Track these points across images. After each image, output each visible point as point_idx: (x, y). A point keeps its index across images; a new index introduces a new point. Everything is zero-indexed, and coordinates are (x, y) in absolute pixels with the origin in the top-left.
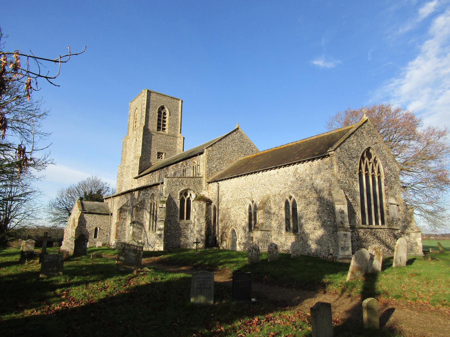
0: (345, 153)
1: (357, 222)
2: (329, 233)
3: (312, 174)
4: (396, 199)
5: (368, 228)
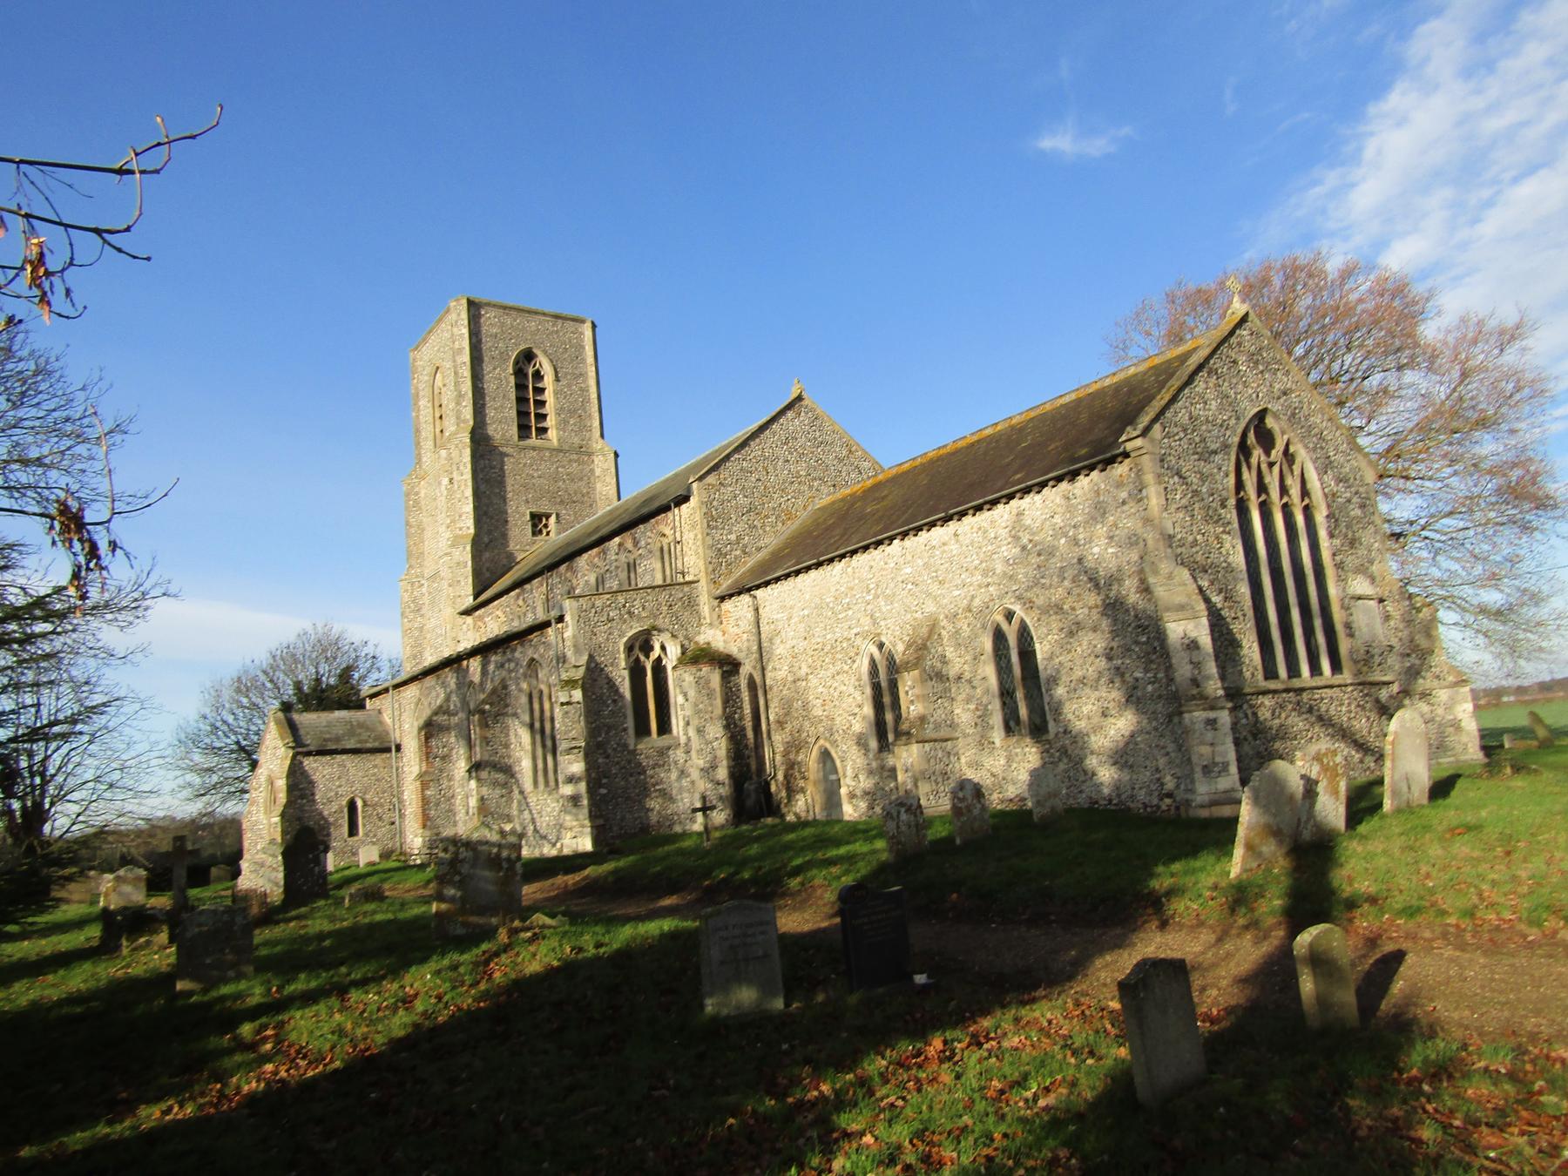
0: (1180, 440)
1: (1247, 675)
2: (1154, 724)
3: (1074, 527)
4: (1373, 579)
5: (1287, 691)
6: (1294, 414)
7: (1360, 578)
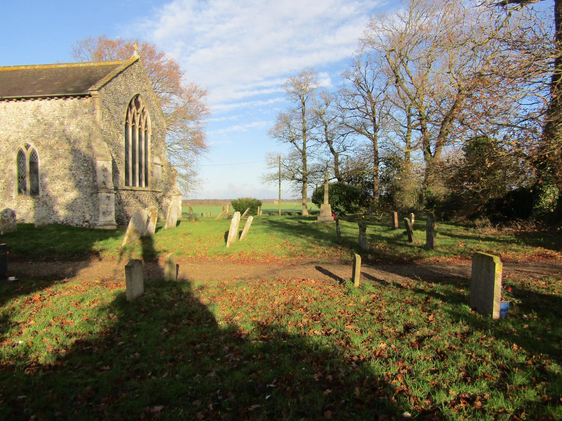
0: (110, 96)
1: (120, 183)
2: (85, 196)
3: (63, 117)
4: (161, 158)
5: (131, 190)
6: (147, 99)
7: (157, 158)
